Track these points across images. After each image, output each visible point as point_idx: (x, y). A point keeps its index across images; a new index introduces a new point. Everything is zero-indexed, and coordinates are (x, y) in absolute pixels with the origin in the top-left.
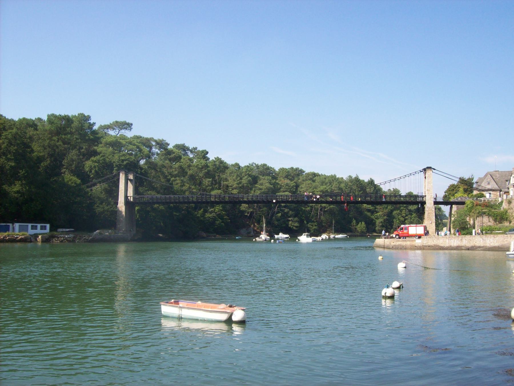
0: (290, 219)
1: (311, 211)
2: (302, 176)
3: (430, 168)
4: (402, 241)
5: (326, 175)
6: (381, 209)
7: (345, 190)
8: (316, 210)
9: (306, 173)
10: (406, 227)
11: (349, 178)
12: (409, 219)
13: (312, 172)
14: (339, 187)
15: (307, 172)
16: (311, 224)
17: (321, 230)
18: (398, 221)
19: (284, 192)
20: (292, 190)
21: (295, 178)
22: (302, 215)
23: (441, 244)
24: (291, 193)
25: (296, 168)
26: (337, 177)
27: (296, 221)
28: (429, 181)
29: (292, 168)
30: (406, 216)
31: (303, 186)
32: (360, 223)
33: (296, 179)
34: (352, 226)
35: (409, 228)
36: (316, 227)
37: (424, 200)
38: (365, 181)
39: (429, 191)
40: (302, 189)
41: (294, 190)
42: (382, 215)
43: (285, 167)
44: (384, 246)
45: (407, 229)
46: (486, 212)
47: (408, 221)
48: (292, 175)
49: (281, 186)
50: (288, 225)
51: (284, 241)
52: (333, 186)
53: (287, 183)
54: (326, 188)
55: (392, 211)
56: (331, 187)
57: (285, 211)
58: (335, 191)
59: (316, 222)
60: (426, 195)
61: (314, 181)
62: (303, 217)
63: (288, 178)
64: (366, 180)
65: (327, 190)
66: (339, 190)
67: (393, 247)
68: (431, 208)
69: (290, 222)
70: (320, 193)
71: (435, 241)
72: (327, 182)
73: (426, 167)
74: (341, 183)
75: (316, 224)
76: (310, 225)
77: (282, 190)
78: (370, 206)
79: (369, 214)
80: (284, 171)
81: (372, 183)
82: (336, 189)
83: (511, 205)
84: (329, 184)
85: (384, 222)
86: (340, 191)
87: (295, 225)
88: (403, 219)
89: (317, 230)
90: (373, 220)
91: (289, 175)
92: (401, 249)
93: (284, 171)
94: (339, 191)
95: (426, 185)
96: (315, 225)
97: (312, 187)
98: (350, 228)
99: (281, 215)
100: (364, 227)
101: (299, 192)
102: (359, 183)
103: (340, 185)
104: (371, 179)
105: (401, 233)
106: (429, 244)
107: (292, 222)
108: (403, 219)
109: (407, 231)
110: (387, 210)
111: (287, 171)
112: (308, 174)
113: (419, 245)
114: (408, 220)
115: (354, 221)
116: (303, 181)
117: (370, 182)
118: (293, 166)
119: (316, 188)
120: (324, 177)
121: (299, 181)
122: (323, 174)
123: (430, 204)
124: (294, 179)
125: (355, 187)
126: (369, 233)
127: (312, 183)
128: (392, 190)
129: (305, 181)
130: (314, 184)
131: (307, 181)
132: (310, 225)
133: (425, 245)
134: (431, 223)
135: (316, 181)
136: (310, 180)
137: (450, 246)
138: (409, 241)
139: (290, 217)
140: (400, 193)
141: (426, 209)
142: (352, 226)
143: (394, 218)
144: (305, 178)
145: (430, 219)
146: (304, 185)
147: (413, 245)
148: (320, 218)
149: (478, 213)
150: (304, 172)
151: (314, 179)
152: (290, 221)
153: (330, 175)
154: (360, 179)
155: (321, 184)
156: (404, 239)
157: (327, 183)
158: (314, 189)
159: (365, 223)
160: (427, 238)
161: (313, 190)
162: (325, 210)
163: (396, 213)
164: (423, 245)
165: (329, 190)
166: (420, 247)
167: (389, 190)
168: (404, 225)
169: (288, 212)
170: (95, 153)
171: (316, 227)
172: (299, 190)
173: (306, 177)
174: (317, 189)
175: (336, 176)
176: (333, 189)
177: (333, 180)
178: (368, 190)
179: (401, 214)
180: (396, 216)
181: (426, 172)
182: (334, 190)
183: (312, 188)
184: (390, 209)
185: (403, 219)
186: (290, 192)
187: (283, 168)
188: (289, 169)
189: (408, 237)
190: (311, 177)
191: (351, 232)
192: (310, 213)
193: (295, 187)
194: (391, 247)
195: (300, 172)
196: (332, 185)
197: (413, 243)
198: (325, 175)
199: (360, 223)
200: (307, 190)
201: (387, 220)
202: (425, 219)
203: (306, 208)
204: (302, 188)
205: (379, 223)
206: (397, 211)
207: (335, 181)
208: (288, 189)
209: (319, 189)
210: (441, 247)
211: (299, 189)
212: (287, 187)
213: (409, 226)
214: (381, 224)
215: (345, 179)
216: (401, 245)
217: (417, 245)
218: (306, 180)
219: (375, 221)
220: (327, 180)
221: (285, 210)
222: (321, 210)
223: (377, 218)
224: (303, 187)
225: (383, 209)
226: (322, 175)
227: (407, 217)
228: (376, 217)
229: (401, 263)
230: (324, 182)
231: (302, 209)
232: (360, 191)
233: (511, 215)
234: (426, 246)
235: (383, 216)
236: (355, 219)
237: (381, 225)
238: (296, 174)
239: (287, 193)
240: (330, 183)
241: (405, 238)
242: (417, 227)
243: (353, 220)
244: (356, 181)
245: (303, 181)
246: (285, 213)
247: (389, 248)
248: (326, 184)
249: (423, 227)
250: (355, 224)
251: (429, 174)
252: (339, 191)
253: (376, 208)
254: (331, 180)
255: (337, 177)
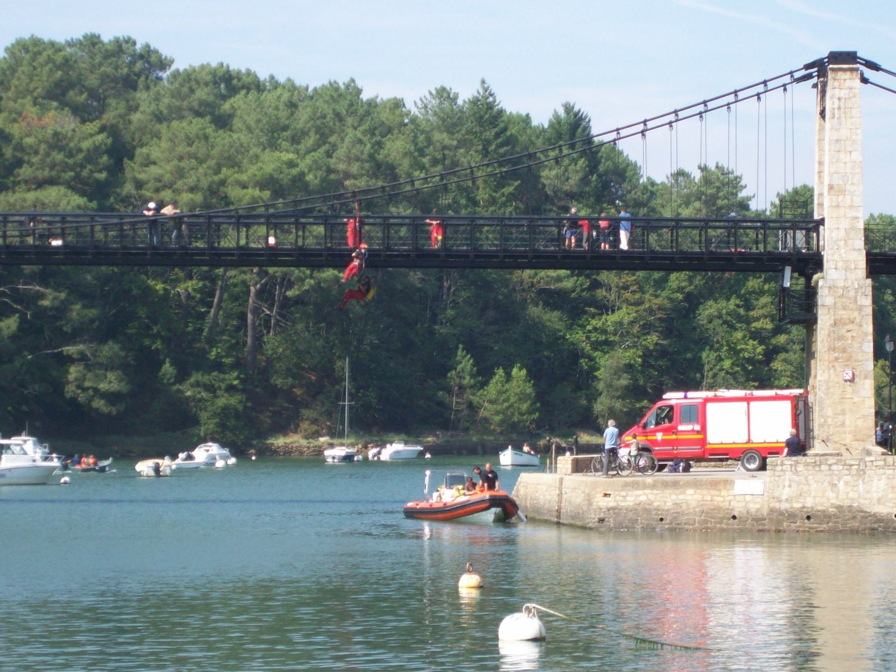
0: (71, 350)
1: (203, 302)
2: (153, 90)
3: (849, 58)
4: (653, 486)
5: (300, 82)
6: (625, 288)
7: (409, 175)
8: (235, 298)
9: (176, 75)
10: (690, 406)
11: (435, 102)
12: (797, 347)
13: (214, 64)
14: (372, 157)
15: (181, 64)
16: (205, 379)
17: (266, 419)
18: (727, 364)
19: (41, 184)
20: (85, 173)
21: (112, 102)
22: (148, 328)
23: (879, 501)
24: (83, 194)
25: (117, 40)
26: (365, 96)
27: (110, 367)
28: (844, 133)
29: (92, 42)
30: (777, 331)
31: (155, 151)
32: (500, 372)
33: (113, 112)
34: (449, 391)
35: (710, 406)
36: (234, 400)
37: (815, 247)
38: (535, 122)
39: (842, 192)
40: (154, 170)
41: (103, 176)
42: (632, 323)
43: (46, 37)
44: (559, 511)
45: (699, 414)
47: (785, 360)
48: (93, 81)
49: (20, 147)
50: (58, 386)
51: (399, 463)
52: (341, 152)
53: (56, 134)
54: (291, 164)
55: (693, 301)
56: (329, 155)
57: (46, 303)
58: (347, 183)
59: (237, 365)
60: (826, 216)
61: (223, 122)
62: (157, 336)
63: (64, 104)
64: (541, 118)
65: (302, 174)
66: (375, 176)
67: (602, 520)
68: (852, 293)
69: (74, 372)
70: (257, 192)
71: (841, 485)
72: (300, 126)
73: (825, 54)
74: (390, 131)
75: (232, 377)
76: (197, 384)
77: (25, 172)
78: (563, 272)
79: (553, 319)
80: (41, 59)
81: (573, 134)
82: (355, 168)
84: (311, 140)
85: (645, 364)
86: (380, 183)
87: (103, 386)
88: (754, 349)
89: (238, 416)
90: (576, 354)
91: (72, 86)
92: (649, 531)
93: (41, 59)
94: (372, 182)
95: (826, 159)
96: (231, 389)
97: (208, 157)
98: (441, 404)
99: (20, 328)
100: (522, 398)
101: (129, 188)
102: (497, 135)
103: (379, 145)
104: (568, 109)
105: (659, 436)
106: (809, 503)
107: (88, 367)
108: (760, 349)
109: (698, 428)
110: (664, 294)
111: (59, 58)
112: (189, 79)
113: (753, 507)
114: (792, 356)
115: (465, 363)
116: (159, 118)
117: (565, 128)
118: (96, 31)
119: (233, 163)
120: (286, 96)
121: (136, 117)
122: (282, 79)
123: (846, 269)
124: (102, 109)
125: (469, 158)
126: (552, 431)
127: (210, 130)
128: (697, 175)
129: (169, 120)
130: (222, 140)
131: (181, 118)
132: (197, 384)
133: (784, 506)
134: (852, 380)
135: (237, 123)
136: (198, 114)
138: (696, 485)
139: (71, 338)
140: (742, 194)
141: (824, 298)
142: (449, 391)
143: (704, 342)
144: (166, 101)
145: (843, 354)
146: (164, 144)
147: (719, 509)
148: (258, 340)
150: (163, 64)
151: (226, 106)
152: (69, 360)
153: (326, 82)
154: (501, 112)
155: (264, 139)
156: (681, 477)
157: (305, 133)
158: (224, 170)
159: (533, 375)
160: (800, 468)
161: (216, 178)
162: (290, 293)
163: (720, 317)
164: (772, 510)
165: (310, 177)
166: (758, 520)
167: (681, 173)
168: (681, 394)
169: (61, 310)
171: (234, 400)
172: (128, 174)
173: (176, 94)
174: (241, 171)
175: (359, 91)
176: (342, 167)
177: (338, 116)
178: (549, 175)
179: (748, 321)
180: (718, 330)
181: (824, 85)
182: (347, 175)
183: (212, 163)
184: (680, 290)
185: (754, 349)
186: (78, 185)
187: (36, 42)
188: (70, 44)
189: (699, 459)
190: (202, 94)
191: (445, 424)
192: (202, 316)
193: (105, 159)
194: (592, 519)
195: (139, 65)
196: (334, 147)
197: (722, 499)
198: (292, 87)
199: (500, 372)
200: (180, 173)
201: (663, 353)
202: (818, 355)
203: (177, 281)
204: (149, 162)
205: (617, 372)
206: (723, 303)
207: (350, 121)
208: (66, 167)
209: (253, 169)
210: (878, 519)
211: (133, 170)
212: (59, 157)
213: (707, 400)
214: (624, 381)
215: (414, 111)
216: (647, 511)
217: (738, 508)
218: (177, 114)
219: (591, 359)
220: (303, 116)
221: (42, 296)
222: (265, 294)
223: (606, 343)
224: (155, 154)
225: (642, 290)
226: (276, 85)
227: (782, 339)
228: (594, 337)
229: (517, 615)
230: (285, 128)
231: (148, 291)
232: (501, 182)
234: (792, 516)
235: (636, 329)
236: (468, 350)
237: (627, 388)
238: (115, 80)
239: (52, 194)
240: (323, 136)
241: (687, 469)
242: (752, 404)
243: (459, 353)
244: (480, 120)
245: (159, 118)
246: (41, 313)
247: (584, 528)
248: (295, 140)
249: (787, 405)
250: (467, 381)
251: (843, 93)
252: (372, 182)
253: (596, 285)
254: (330, 116)
255: (365, 96)
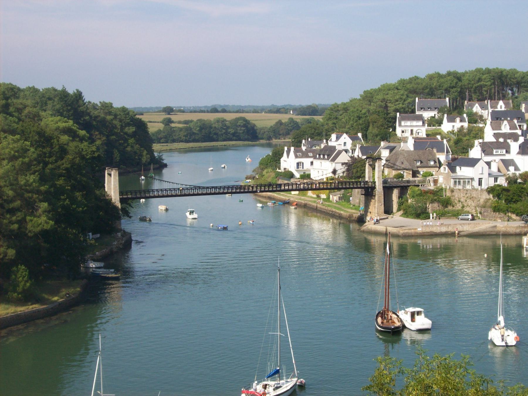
46: (436, 199)
83: (453, 194)
106: (427, 231)
113: (420, 232)
137: (441, 232)
149: (432, 200)
170: (399, 210)
217: (418, 232)
233: (453, 201)
